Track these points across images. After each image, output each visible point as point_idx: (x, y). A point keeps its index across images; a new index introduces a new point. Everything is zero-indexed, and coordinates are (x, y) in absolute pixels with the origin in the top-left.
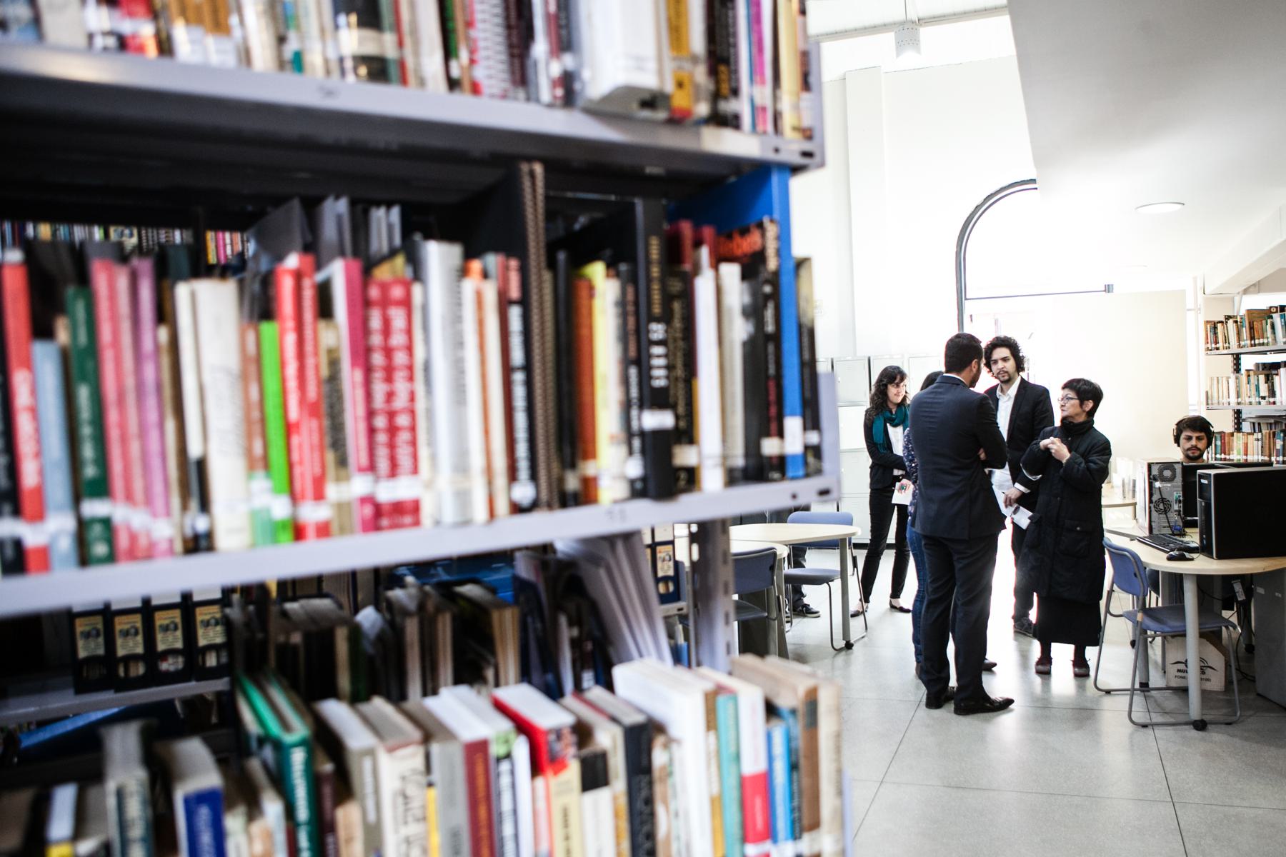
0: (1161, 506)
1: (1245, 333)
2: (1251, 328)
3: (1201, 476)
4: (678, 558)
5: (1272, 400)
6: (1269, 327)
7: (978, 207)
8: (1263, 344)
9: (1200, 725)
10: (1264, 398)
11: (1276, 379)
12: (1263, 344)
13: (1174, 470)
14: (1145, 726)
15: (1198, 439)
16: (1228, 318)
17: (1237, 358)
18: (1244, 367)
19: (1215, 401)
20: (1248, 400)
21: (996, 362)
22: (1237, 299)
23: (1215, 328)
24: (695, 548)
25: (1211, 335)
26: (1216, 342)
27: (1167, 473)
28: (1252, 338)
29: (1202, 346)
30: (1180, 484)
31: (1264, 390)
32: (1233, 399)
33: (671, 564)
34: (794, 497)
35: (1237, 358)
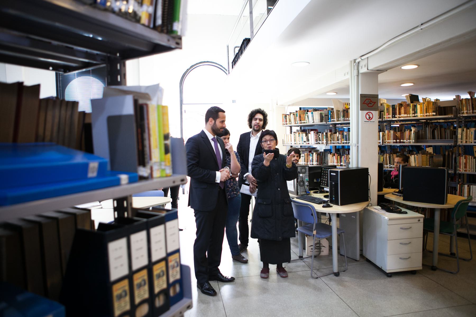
0: (302, 183)
1: (298, 118)
2: (300, 117)
3: (331, 172)
4: (184, 262)
5: (308, 142)
6: (307, 117)
7: (204, 62)
8: (305, 123)
9: (337, 274)
10: (305, 142)
11: (309, 135)
12: (305, 123)
13: (306, 169)
14: (317, 278)
15: (297, 156)
16: (291, 113)
17: (291, 127)
18: (293, 131)
19: (286, 143)
20: (299, 142)
21: (256, 119)
22: (286, 108)
23: (286, 116)
24: (116, 213)
25: (284, 119)
26: (286, 122)
27: (303, 170)
28: (300, 120)
29: (282, 123)
30: (308, 174)
31: (305, 139)
32: (290, 142)
33: (178, 269)
34: (174, 182)
35: (291, 127)
